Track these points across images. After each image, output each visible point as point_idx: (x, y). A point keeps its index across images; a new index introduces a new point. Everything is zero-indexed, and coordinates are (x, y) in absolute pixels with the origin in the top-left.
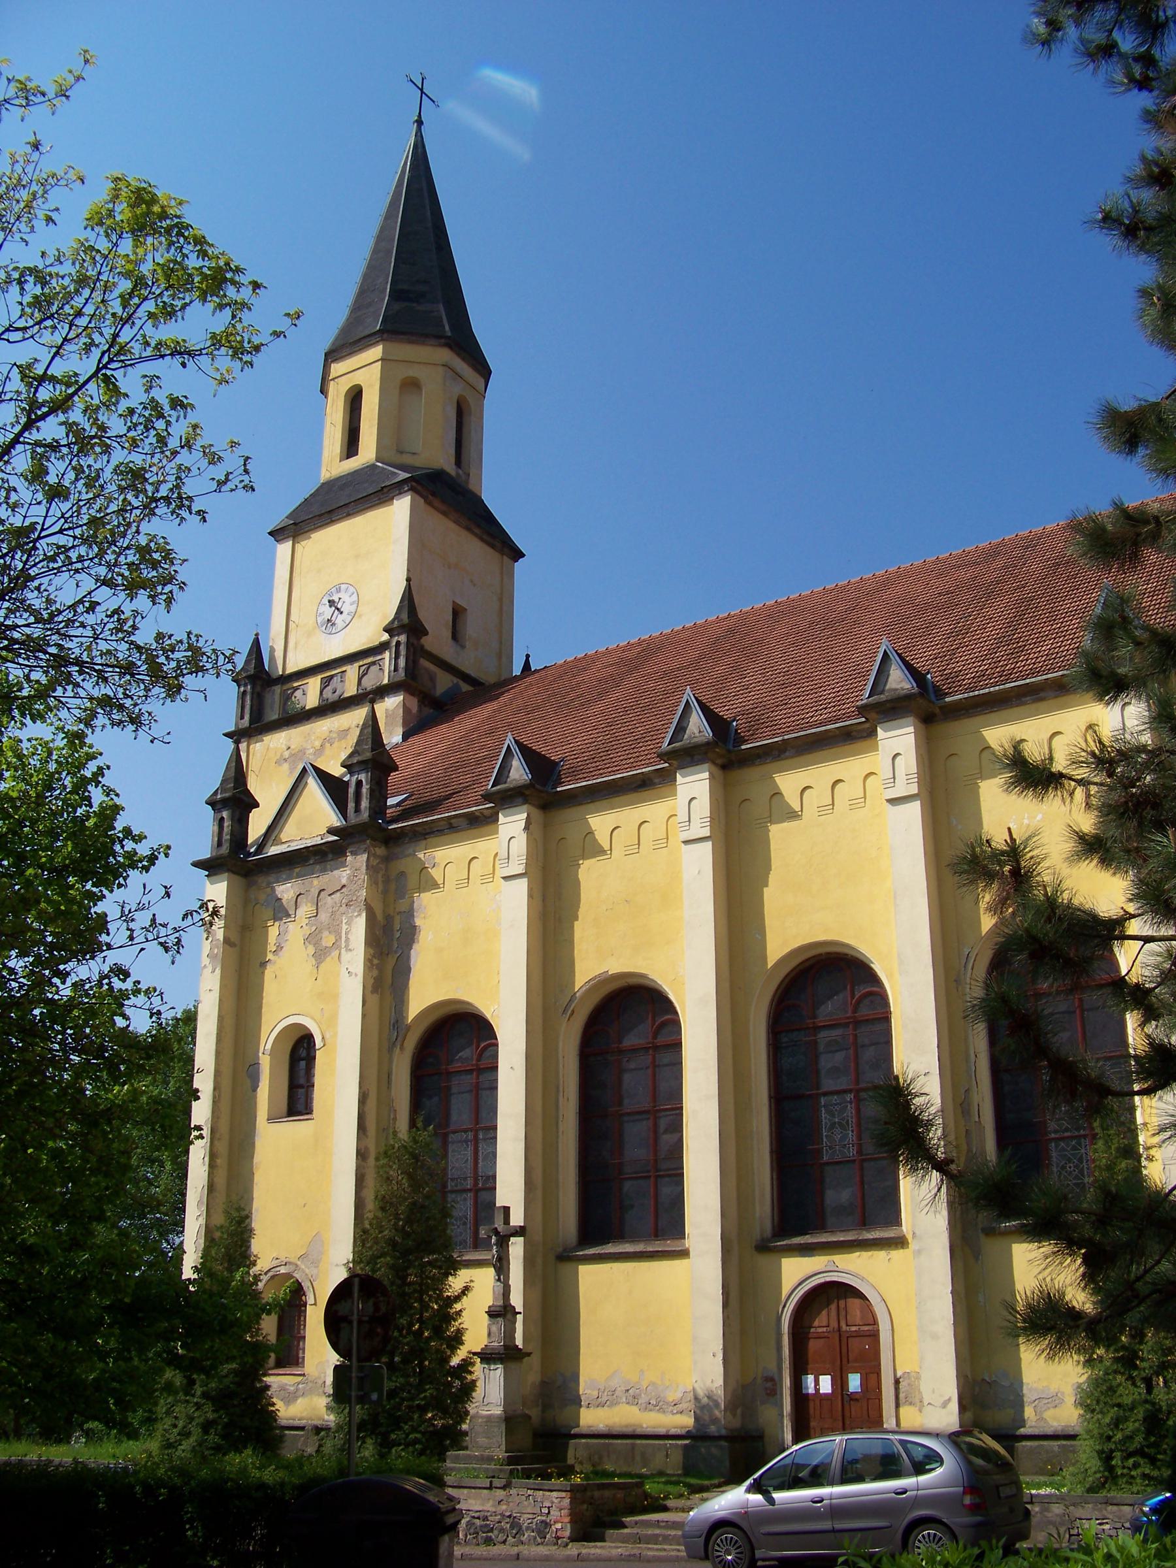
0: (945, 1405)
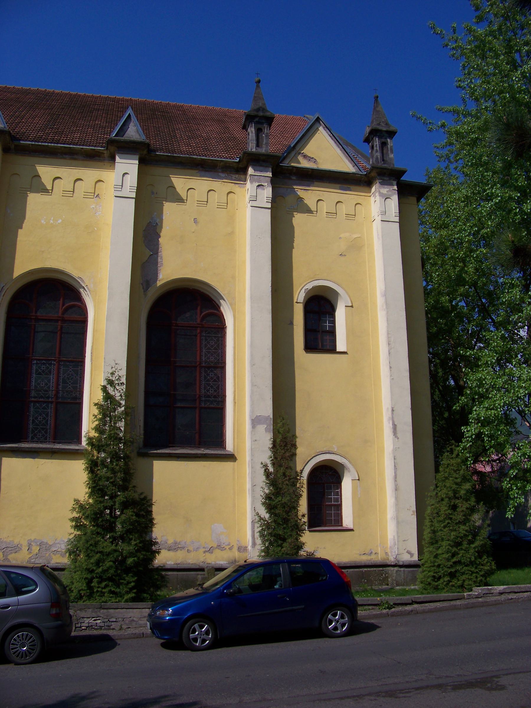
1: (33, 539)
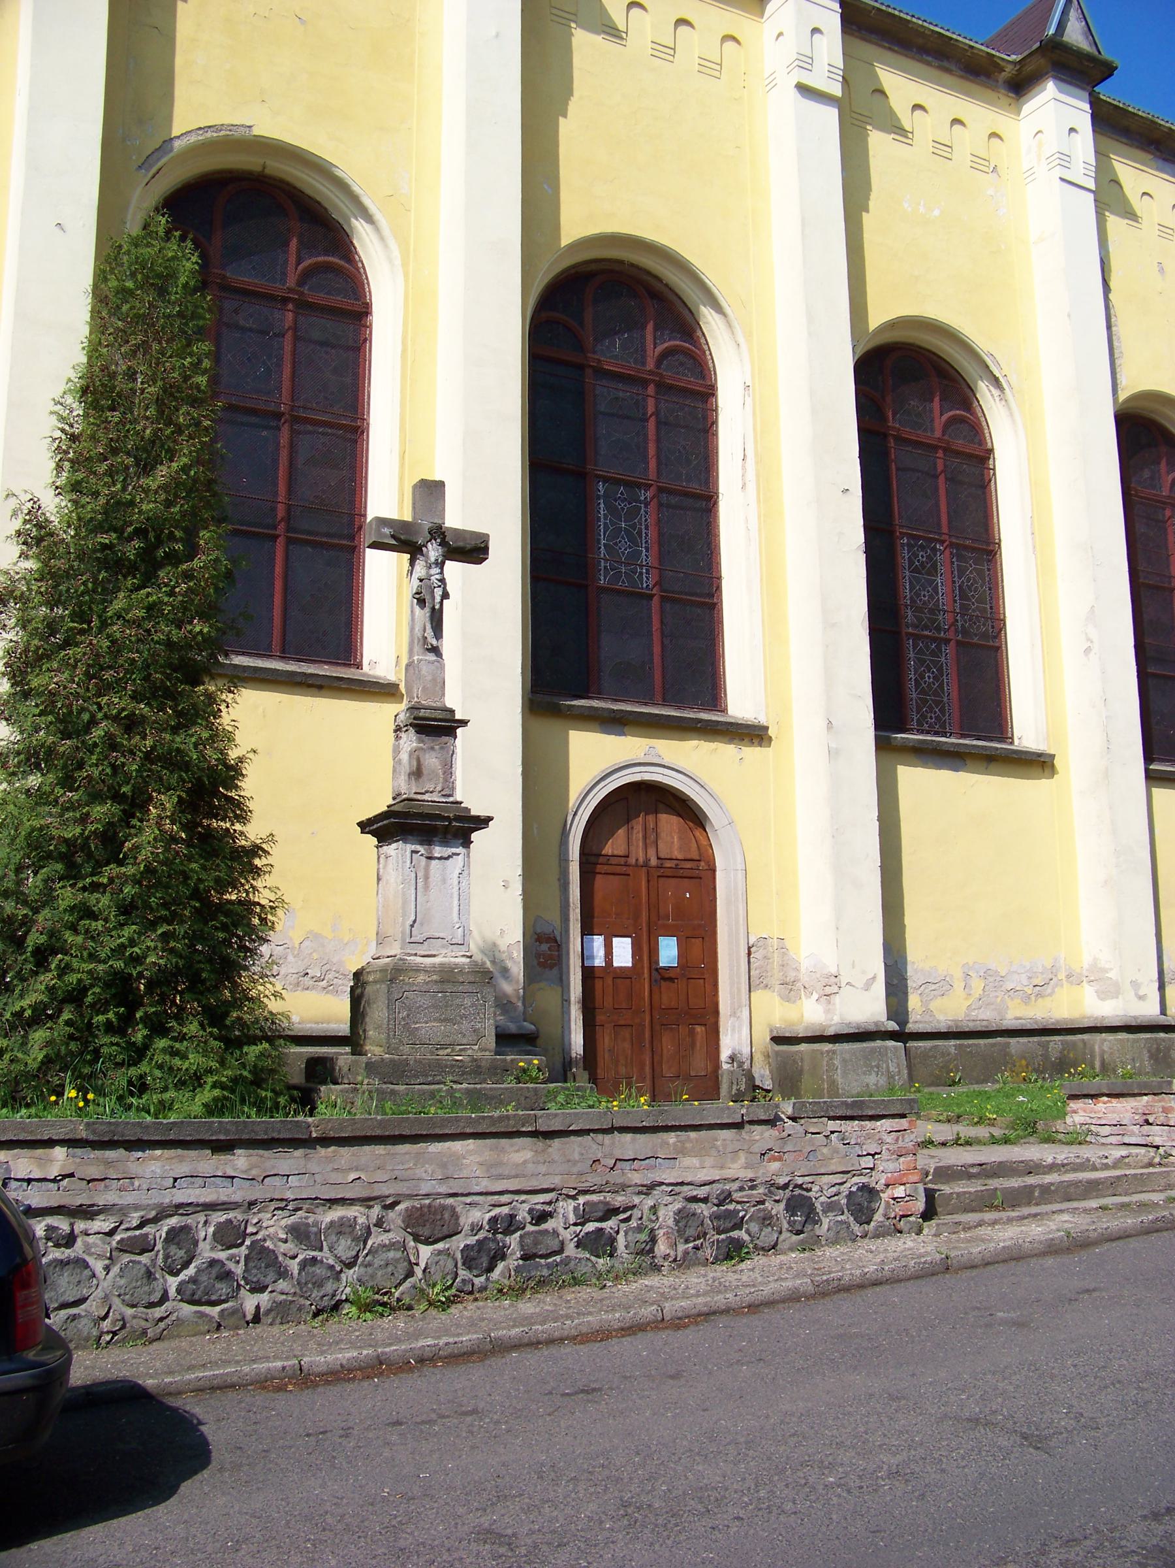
0: (868, 986)
1: (971, 964)
